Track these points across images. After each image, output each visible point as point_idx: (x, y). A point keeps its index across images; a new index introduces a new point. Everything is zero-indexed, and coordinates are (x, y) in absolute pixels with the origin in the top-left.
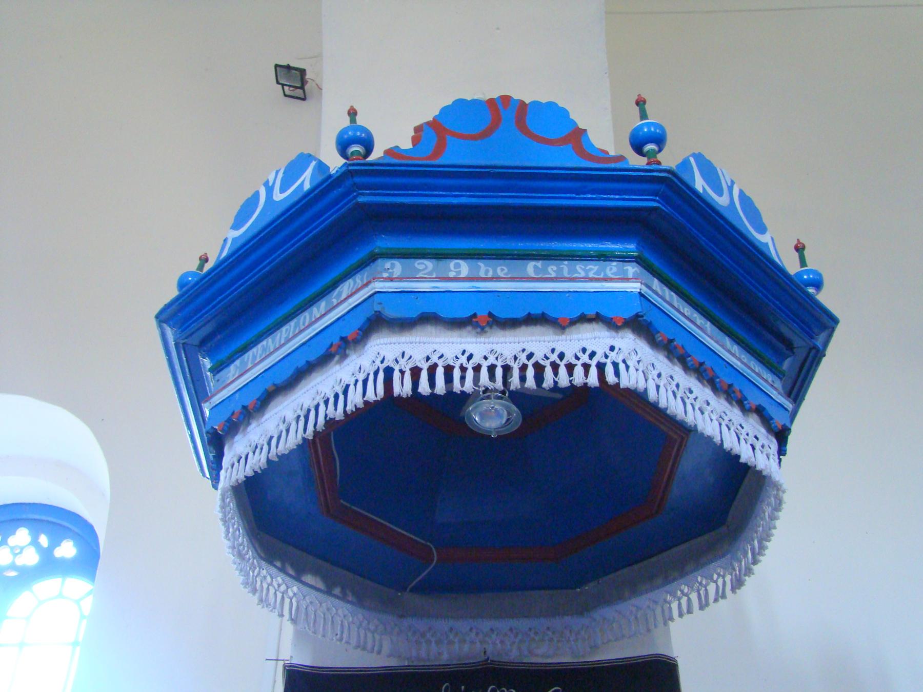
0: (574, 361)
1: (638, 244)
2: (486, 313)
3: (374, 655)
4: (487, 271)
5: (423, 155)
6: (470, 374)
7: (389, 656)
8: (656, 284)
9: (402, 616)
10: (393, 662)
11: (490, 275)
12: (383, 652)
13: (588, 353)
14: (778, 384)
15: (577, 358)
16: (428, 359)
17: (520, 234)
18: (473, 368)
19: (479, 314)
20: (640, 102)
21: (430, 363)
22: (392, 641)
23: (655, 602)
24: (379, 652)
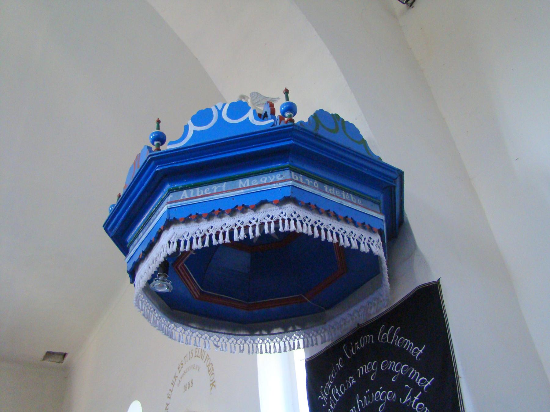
0: (249, 224)
1: (169, 183)
2: (195, 214)
3: (315, 346)
4: (200, 193)
5: (312, 129)
6: (242, 230)
7: (322, 343)
8: (301, 178)
9: (325, 323)
10: (327, 344)
11: (202, 194)
12: (318, 343)
13: (270, 217)
14: (377, 207)
15: (250, 223)
16: (236, 225)
17: (235, 169)
18: (274, 222)
19: (239, 206)
20: (159, 122)
21: (237, 227)
22: (321, 336)
23: (272, 340)
24: (317, 344)
